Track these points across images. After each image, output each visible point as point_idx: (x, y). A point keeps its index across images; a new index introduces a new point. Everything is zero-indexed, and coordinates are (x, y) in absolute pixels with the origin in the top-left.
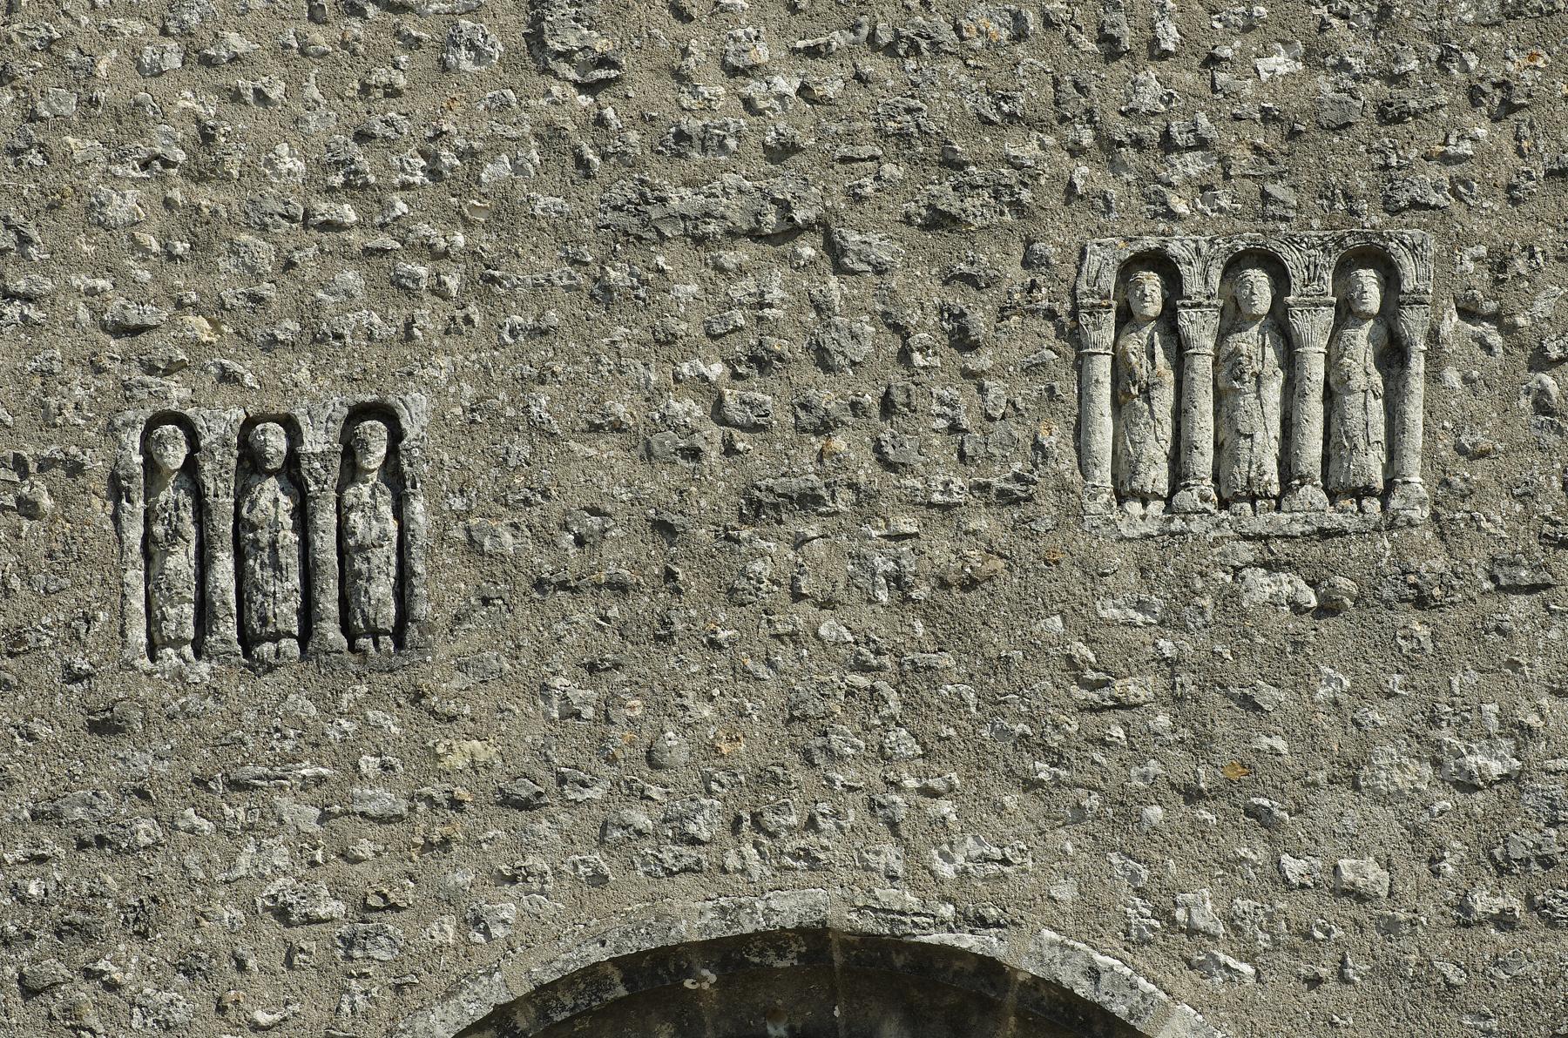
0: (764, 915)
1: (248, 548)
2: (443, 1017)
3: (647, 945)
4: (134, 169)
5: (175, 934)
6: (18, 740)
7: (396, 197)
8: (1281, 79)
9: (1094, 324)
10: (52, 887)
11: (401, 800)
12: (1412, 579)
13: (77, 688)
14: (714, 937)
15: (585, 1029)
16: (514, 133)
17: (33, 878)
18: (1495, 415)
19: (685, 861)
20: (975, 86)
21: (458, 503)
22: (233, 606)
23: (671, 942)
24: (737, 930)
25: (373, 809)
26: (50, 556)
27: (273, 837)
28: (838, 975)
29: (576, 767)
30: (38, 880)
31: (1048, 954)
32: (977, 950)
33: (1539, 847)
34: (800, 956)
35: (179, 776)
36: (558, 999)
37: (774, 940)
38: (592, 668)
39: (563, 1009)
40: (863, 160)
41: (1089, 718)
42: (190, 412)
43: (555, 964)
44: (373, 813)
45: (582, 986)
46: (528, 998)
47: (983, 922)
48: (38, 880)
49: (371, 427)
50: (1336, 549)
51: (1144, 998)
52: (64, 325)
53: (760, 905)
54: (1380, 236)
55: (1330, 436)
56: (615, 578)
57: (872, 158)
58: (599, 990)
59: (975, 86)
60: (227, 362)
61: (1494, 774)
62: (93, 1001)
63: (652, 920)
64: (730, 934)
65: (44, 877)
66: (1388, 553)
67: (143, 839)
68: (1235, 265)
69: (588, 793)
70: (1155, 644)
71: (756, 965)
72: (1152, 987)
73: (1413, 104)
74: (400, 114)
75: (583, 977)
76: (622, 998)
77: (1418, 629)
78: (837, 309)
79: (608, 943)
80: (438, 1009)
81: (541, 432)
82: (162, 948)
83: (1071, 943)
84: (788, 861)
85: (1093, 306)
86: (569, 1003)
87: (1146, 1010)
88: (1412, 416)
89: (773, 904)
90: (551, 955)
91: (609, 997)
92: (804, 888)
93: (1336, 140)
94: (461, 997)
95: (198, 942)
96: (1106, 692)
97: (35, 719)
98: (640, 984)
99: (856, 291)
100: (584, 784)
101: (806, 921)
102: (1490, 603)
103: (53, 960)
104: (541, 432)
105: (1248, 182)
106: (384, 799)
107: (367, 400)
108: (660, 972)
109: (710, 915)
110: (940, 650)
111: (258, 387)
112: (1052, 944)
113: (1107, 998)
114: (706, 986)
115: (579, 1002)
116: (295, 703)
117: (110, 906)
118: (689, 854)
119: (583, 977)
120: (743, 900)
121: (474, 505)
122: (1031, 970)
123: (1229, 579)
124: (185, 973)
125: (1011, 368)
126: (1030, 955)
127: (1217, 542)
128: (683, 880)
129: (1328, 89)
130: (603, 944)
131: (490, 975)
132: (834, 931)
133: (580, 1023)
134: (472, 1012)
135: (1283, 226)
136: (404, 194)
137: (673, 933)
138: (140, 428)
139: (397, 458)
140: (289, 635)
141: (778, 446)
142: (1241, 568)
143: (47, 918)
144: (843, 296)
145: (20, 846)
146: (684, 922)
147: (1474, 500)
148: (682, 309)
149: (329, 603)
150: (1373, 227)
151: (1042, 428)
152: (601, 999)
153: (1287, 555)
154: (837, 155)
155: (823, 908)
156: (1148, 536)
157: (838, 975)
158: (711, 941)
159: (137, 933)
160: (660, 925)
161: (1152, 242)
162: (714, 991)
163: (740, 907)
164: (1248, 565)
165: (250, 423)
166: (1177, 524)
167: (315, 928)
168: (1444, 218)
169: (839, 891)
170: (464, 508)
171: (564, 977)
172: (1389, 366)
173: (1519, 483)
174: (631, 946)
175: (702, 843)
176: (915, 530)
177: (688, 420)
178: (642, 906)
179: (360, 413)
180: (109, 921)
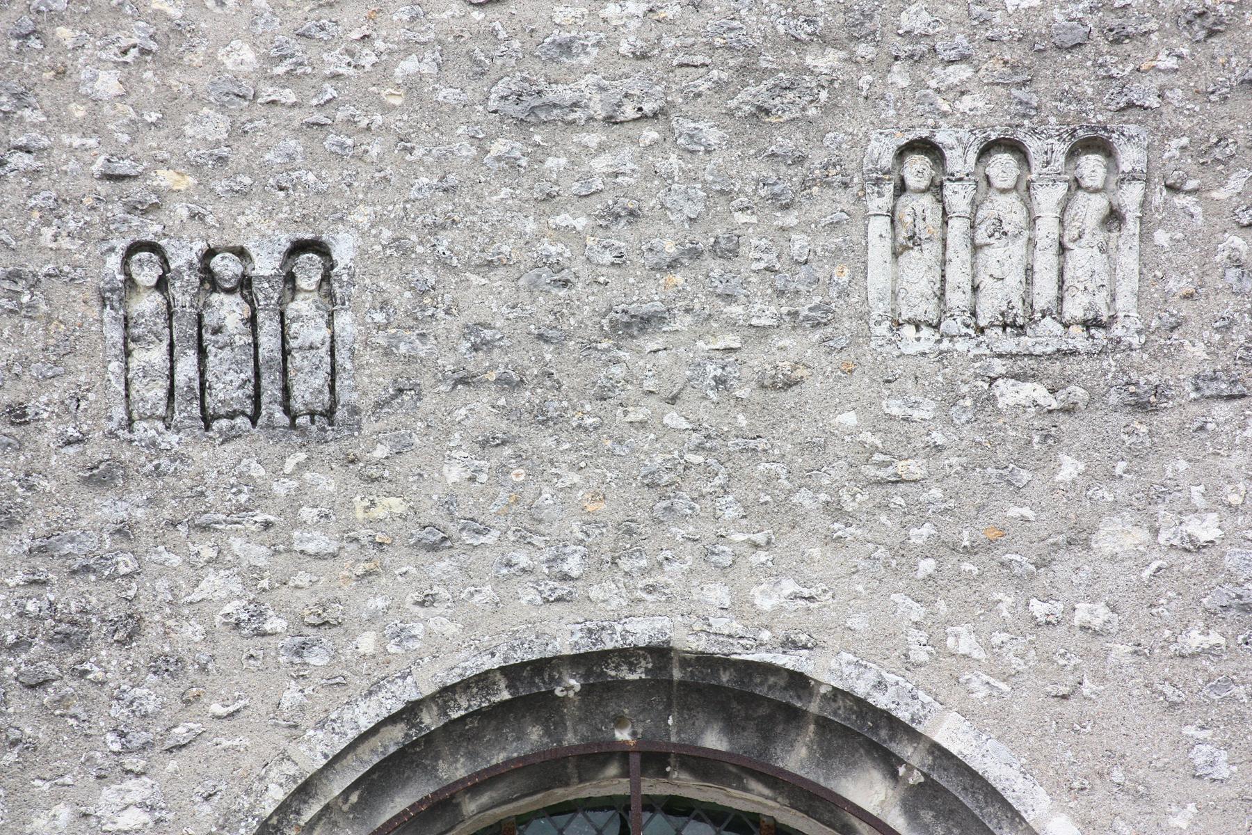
0: (621, 635)
1: (210, 347)
2: (365, 710)
3: (529, 657)
4: (116, 55)
5: (151, 641)
6: (19, 490)
7: (326, 85)
8: (1023, 12)
9: (878, 193)
10: (45, 605)
11: (333, 542)
12: (1132, 389)
13: (71, 450)
14: (582, 651)
15: (474, 727)
16: (422, 39)
17: (29, 598)
18: (1196, 267)
19: (558, 593)
20: (783, 13)
21: (380, 317)
22: (198, 392)
23: (548, 655)
24: (600, 647)
25: (311, 548)
26: (45, 349)
27: (229, 569)
28: (675, 688)
29: (472, 519)
30: (34, 600)
31: (847, 671)
32: (789, 666)
33: (1240, 597)
34: (647, 671)
35: (153, 521)
36: (456, 701)
37: (627, 655)
38: (484, 444)
39: (459, 708)
40: (696, 66)
41: (877, 490)
42: (163, 242)
43: (456, 670)
44: (311, 552)
45: (475, 690)
46: (432, 698)
47: (795, 645)
48: (34, 600)
49: (308, 258)
50: (1072, 367)
51: (923, 706)
52: (58, 172)
53: (619, 628)
54: (1105, 129)
55: (1063, 282)
56: (504, 376)
57: (703, 65)
58: (488, 694)
59: (783, 13)
60: (193, 206)
61: (1202, 541)
62: (79, 695)
63: (533, 637)
64: (595, 649)
65: (39, 597)
66: (1113, 369)
67: (123, 570)
68: (987, 150)
69: (482, 539)
70: (1180, 57)
71: (612, 677)
72: (928, 699)
73: (1130, 29)
74: (330, 21)
75: (477, 682)
76: (506, 701)
77: (1138, 427)
78: (676, 179)
79: (498, 655)
80: (361, 704)
81: (445, 265)
82: (138, 653)
83: (864, 663)
84: (640, 594)
85: (878, 179)
86: (464, 704)
87: (925, 716)
88: (397, 800)
89: (628, 627)
90: (453, 663)
91: (496, 699)
92: (653, 616)
93: (1068, 57)
94: (380, 695)
95: (167, 649)
96: (890, 470)
97: (34, 475)
98: (521, 690)
99: (690, 166)
100: (478, 532)
101: (655, 642)
102: (1194, 409)
103: (46, 663)
104: (445, 265)
105: (997, 88)
106: (318, 542)
107: (306, 238)
108: (537, 681)
109: (580, 634)
110: (758, 437)
111: (218, 225)
112: (849, 663)
113: (893, 706)
114: (571, 694)
115: (472, 703)
116: (248, 466)
117: (94, 620)
118: (563, 588)
119: (477, 682)
120: (605, 624)
121: (392, 319)
122: (833, 683)
123: (986, 386)
124: (155, 673)
125: (813, 226)
126: (831, 671)
127: (977, 358)
128: (557, 608)
129: (1060, 18)
130: (493, 655)
131: (404, 678)
132: (676, 651)
133: (472, 722)
134: (389, 707)
135: (1026, 122)
136: (334, 82)
137: (550, 647)
138: (120, 252)
139: (329, 283)
140: (243, 413)
141: (631, 280)
142: (996, 379)
143: (41, 629)
144: (681, 169)
145: (19, 573)
146: (559, 639)
147: (1181, 331)
148: (555, 177)
149: (271, 389)
150: (1099, 122)
151: (836, 271)
152: (490, 701)
153: (1032, 369)
154: (675, 63)
155: (668, 631)
156: (923, 354)
157: (675, 688)
158: (580, 655)
159: (117, 641)
160: (539, 641)
161: (925, 133)
162: (577, 699)
163: (603, 629)
164: (1002, 376)
165: (210, 253)
166: (945, 345)
167: (264, 640)
168: (1155, 117)
169: (680, 619)
170: (385, 321)
171: (462, 681)
172: (1110, 231)
173: (1217, 318)
174: (519, 656)
175: (572, 579)
176: (739, 345)
177: (560, 259)
178: (524, 627)
179: (299, 247)
180: (98, 629)
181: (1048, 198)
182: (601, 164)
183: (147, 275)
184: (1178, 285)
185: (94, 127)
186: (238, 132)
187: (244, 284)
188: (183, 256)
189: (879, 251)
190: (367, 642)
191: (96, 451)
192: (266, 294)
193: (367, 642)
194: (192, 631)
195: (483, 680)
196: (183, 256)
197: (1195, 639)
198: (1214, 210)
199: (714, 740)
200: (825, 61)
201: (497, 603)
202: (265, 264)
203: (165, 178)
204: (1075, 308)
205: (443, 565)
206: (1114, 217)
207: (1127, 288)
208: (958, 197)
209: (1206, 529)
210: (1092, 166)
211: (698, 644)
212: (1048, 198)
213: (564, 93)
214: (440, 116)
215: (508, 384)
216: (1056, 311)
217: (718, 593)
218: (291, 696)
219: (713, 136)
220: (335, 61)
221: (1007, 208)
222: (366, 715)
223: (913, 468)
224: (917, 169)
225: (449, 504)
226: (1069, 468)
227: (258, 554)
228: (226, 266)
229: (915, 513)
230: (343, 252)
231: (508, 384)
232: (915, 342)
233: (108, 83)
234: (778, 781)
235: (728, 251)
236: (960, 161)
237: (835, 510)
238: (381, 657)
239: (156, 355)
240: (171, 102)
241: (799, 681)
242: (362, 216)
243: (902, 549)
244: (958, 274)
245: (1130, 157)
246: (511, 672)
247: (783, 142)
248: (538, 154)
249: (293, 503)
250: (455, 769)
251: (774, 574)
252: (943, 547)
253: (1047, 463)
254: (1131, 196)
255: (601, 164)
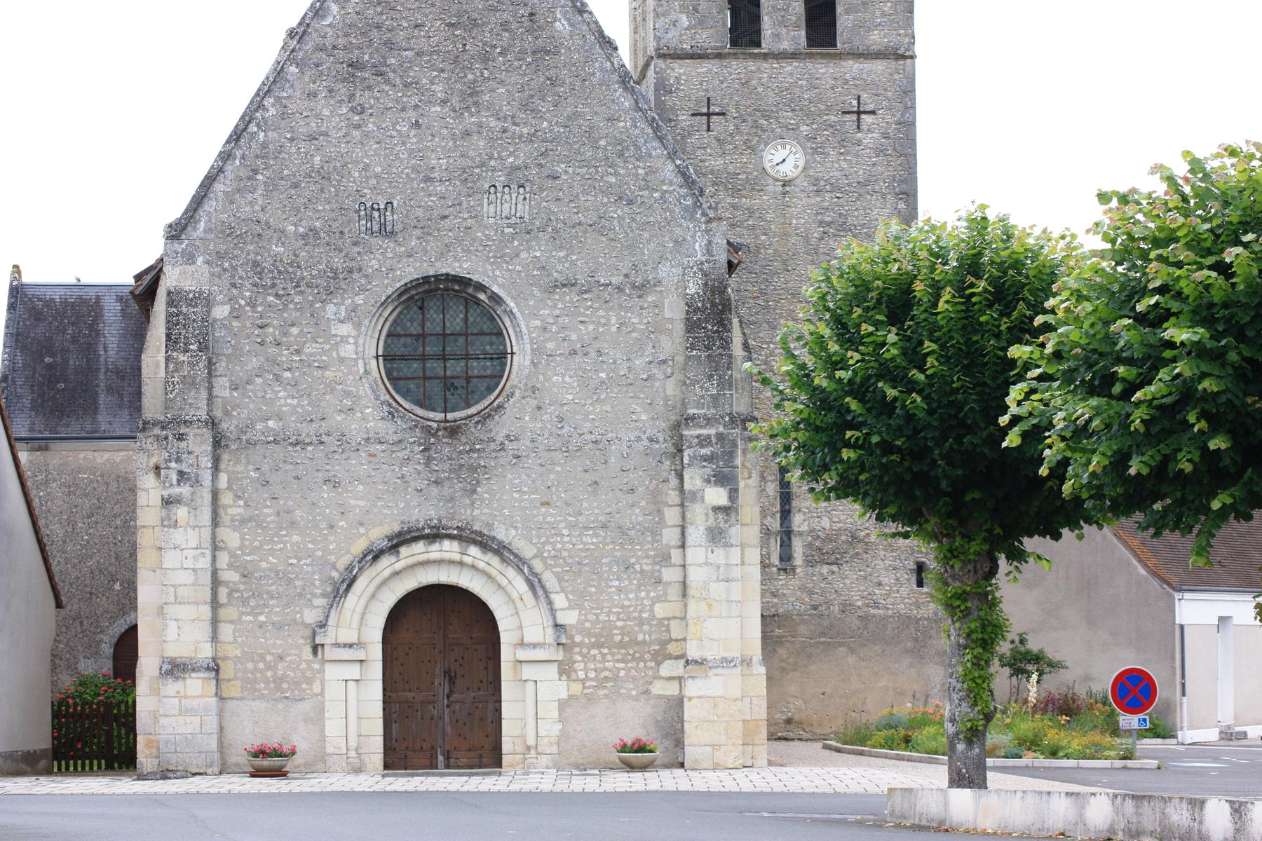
37: (442, 275)
106: (390, 255)
181: (514, 196)
182: (439, 188)
183: (363, 208)
184: (535, 211)
185: (354, 182)
186: (378, 183)
187: (379, 209)
188: (369, 205)
189: (485, 205)
190: (398, 273)
191: (354, 239)
192: (382, 211)
193: (398, 273)
194: (370, 270)
195: (418, 279)
196: (369, 205)
197: (535, 273)
198: (541, 198)
199: (457, 287)
200: (477, 171)
201: (529, 748)
202: (382, 207)
203: (366, 191)
204: (518, 215)
205: (411, 259)
206: (525, 199)
207: (527, 211)
208: (499, 195)
209: (538, 254)
210: (521, 190)
211: (453, 273)
212: (514, 196)
213: (433, 176)
214: (412, 180)
215: (422, 228)
216: (515, 215)
217: (457, 264)
218: (386, 281)
219: (458, 183)
220: (394, 170)
221: (507, 197)
222: (398, 285)
223: (490, 243)
224: (492, 190)
225: (412, 249)
226: (516, 243)
227: (381, 257)
228: (375, 206)
229: (490, 251)
230: (395, 205)
231: (422, 228)
232: (491, 221)
233: (357, 174)
234: (467, 294)
235: (460, 204)
236: (500, 189)
237: (477, 250)
238: (401, 275)
239: (364, 222)
240: (367, 178)
241: (470, 279)
242: (398, 198)
243: (488, 257)
244: (499, 209)
245: (528, 189)
246: (422, 278)
247: (469, 185)
248: (428, 187)
249: (386, 248)
250: (414, 292)
251: (467, 261)
252: (495, 257)
253: (512, 242)
254: (528, 196)
255: (439, 188)
